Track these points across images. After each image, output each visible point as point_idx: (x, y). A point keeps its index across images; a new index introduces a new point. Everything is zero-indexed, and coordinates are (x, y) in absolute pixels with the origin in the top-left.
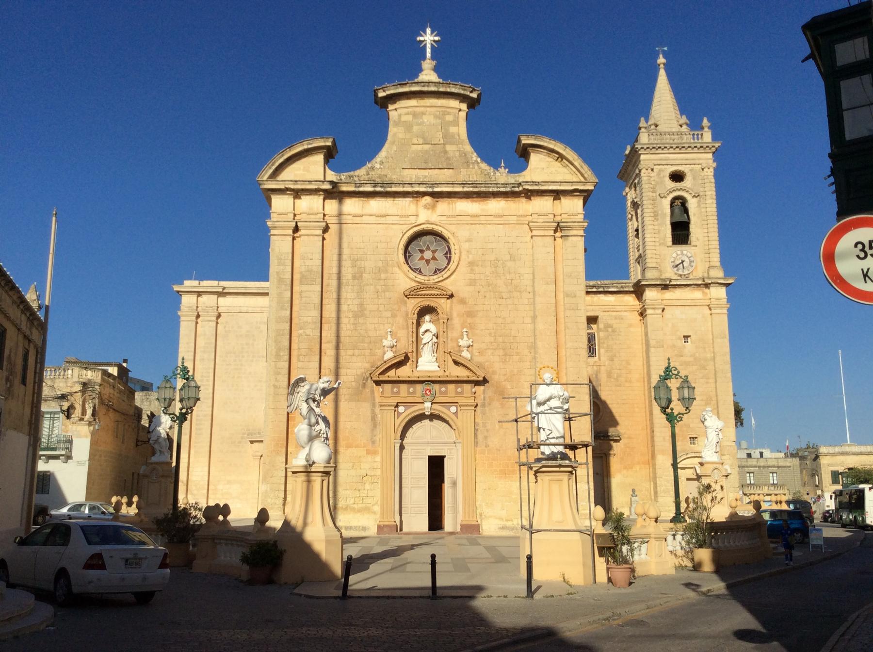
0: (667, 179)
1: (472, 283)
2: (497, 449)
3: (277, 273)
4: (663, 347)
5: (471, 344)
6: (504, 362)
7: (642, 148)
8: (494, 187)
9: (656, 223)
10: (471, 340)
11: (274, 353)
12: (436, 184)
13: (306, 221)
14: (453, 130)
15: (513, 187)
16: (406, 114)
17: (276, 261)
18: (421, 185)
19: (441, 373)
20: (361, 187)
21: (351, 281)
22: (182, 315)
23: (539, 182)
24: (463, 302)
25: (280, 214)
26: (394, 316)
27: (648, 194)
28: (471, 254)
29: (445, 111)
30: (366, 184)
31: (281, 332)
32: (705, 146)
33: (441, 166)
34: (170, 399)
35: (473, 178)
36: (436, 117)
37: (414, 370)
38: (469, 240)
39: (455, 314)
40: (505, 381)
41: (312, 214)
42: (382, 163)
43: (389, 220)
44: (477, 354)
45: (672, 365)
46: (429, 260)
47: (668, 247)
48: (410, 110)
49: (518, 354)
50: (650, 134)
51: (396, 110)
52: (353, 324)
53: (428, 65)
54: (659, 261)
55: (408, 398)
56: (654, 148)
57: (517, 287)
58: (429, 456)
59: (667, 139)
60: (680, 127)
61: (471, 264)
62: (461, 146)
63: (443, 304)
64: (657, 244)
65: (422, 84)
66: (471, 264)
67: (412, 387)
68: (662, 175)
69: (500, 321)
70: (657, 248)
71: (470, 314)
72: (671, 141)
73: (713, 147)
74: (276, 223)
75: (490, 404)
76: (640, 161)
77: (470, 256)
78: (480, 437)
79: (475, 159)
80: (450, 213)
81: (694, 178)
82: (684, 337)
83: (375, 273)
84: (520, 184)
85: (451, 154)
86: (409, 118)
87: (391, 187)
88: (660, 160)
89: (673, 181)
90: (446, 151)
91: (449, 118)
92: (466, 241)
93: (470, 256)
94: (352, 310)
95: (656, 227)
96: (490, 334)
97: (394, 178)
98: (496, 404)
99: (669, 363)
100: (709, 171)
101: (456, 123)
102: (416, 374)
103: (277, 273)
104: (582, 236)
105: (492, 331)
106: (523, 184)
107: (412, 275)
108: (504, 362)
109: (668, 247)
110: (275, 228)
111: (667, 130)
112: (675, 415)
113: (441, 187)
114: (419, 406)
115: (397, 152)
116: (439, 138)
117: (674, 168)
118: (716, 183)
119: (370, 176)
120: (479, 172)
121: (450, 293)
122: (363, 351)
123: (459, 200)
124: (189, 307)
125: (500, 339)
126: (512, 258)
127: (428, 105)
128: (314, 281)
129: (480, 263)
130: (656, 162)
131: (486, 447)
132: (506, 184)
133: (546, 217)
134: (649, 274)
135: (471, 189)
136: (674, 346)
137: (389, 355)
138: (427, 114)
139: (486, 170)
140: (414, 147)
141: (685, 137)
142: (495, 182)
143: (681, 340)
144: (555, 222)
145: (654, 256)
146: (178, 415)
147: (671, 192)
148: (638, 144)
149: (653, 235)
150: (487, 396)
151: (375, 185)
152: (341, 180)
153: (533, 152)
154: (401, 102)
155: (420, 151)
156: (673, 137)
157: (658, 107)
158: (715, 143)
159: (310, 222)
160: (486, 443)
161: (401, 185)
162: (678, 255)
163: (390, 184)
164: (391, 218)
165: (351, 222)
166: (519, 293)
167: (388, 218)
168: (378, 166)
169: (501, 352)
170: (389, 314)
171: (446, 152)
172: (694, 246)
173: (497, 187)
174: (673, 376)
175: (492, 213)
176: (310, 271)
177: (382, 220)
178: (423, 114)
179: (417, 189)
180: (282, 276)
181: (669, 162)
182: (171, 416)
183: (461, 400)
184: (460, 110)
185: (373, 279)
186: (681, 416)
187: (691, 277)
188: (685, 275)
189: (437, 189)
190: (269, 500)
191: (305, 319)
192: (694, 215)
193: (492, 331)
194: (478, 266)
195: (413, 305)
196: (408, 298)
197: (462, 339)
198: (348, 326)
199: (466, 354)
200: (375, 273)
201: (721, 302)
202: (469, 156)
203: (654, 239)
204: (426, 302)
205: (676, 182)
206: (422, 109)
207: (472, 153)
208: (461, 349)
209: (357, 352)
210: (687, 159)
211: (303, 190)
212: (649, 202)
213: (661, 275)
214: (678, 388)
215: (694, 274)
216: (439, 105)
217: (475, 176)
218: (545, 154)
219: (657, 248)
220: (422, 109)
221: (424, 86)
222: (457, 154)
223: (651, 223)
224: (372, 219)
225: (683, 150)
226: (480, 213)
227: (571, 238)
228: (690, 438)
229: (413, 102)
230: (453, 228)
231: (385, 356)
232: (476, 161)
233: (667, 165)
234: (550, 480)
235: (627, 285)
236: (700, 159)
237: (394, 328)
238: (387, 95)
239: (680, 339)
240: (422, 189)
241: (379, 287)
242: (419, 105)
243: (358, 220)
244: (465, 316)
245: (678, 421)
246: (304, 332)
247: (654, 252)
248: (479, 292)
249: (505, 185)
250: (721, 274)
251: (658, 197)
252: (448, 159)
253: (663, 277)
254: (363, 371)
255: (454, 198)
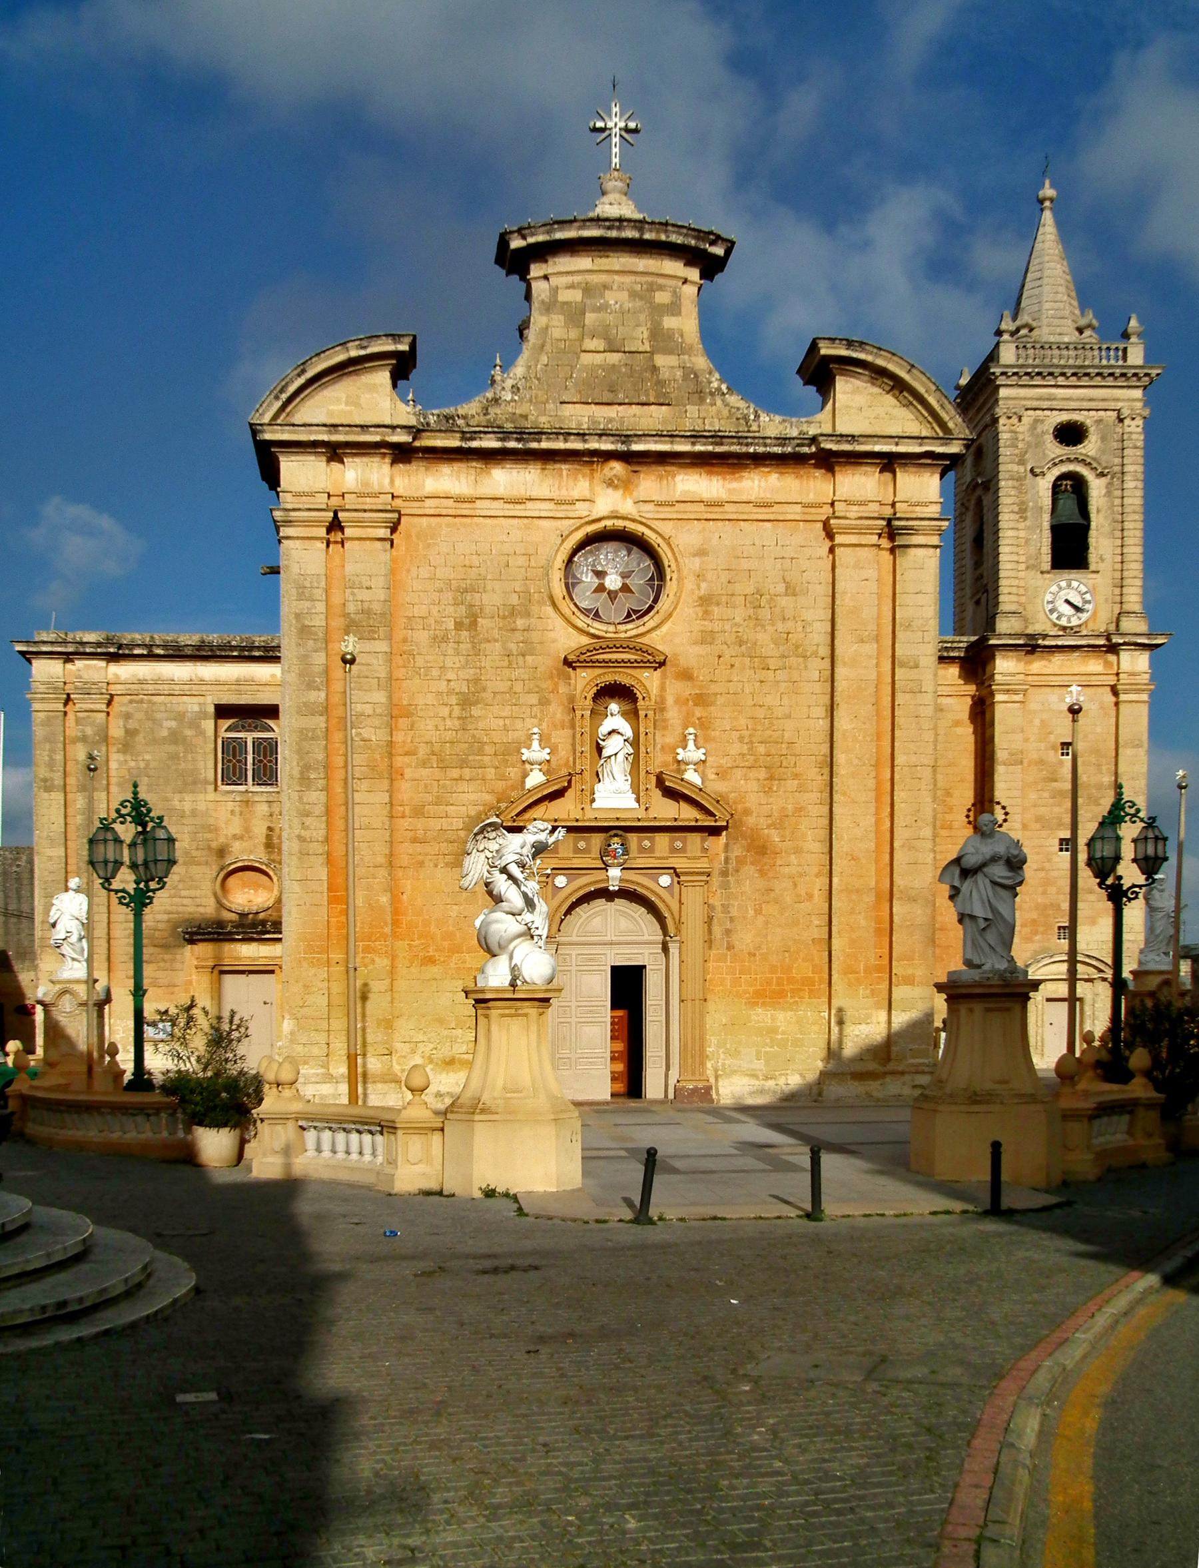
0: (1049, 438)
1: (707, 638)
2: (749, 954)
3: (298, 616)
4: (1021, 763)
5: (703, 758)
6: (768, 791)
7: (1003, 374)
8: (757, 444)
9: (1022, 525)
10: (703, 750)
11: (296, 772)
12: (636, 435)
13: (356, 510)
14: (669, 322)
15: (798, 445)
16: (568, 288)
17: (294, 591)
18: (604, 438)
19: (641, 814)
20: (474, 439)
21: (453, 633)
22: (35, 699)
23: (853, 436)
24: (686, 675)
25: (298, 495)
26: (544, 702)
27: (1010, 467)
28: (704, 580)
29: (652, 284)
30: (485, 433)
31: (310, 734)
32: (1057, 371)
33: (643, 399)
34: (116, 862)
35: (711, 424)
36: (633, 295)
37: (587, 807)
38: (701, 553)
39: (670, 701)
40: (768, 827)
41: (369, 495)
42: (515, 389)
43: (533, 509)
44: (713, 776)
45: (1126, 798)
46: (616, 592)
47: (1042, 573)
48: (577, 279)
49: (796, 776)
50: (1021, 345)
51: (546, 277)
52: (459, 718)
53: (614, 184)
54: (1023, 599)
55: (575, 861)
56: (1027, 374)
57: (797, 647)
58: (614, 969)
59: (1056, 358)
60: (1077, 333)
61: (705, 601)
62: (686, 357)
63: (648, 682)
64: (1022, 567)
65: (607, 224)
66: (705, 601)
67: (583, 839)
68: (1039, 430)
69: (760, 713)
70: (1021, 574)
71: (701, 700)
72: (1062, 362)
73: (1146, 375)
74: (292, 514)
75: (737, 871)
76: (997, 401)
77: (704, 585)
78: (717, 931)
79: (715, 385)
80: (663, 498)
81: (1103, 439)
82: (1063, 744)
83: (504, 617)
84: (814, 440)
85: (665, 374)
86: (576, 296)
87: (539, 441)
88: (1038, 399)
89: (1061, 442)
90: (654, 366)
91: (662, 298)
92: (695, 555)
93: (704, 585)
94: (457, 690)
95: (1022, 534)
96: (741, 739)
97: (544, 422)
98: (749, 870)
99: (1119, 795)
100: (1133, 423)
101: (674, 308)
102: (590, 814)
103: (298, 616)
104: (936, 547)
105: (746, 733)
106: (821, 438)
107: (581, 621)
108: (768, 791)
109: (1042, 573)
110: (288, 523)
111: (1052, 339)
112: (1125, 888)
113: (646, 442)
114: (600, 875)
115: (549, 368)
116: (640, 338)
117: (1064, 417)
118: (1145, 448)
119: (491, 417)
120: (725, 412)
121: (661, 658)
122: (480, 771)
123: (682, 471)
124: (49, 683)
125: (762, 749)
126: (791, 590)
127: (617, 268)
128: (375, 632)
129: (724, 599)
130: (1029, 404)
131: (728, 949)
132: (785, 439)
133: (862, 508)
134: (1002, 625)
135: (710, 448)
136: (1041, 762)
137: (535, 778)
138: (615, 287)
139: (738, 409)
140: (586, 359)
141: (1089, 354)
142: (757, 434)
143: (1056, 751)
144: (883, 519)
145: (1014, 590)
146: (132, 892)
147: (1055, 464)
148: (995, 367)
149: (1015, 549)
150: (733, 855)
151: (505, 435)
152: (428, 424)
153: (841, 375)
154: (556, 260)
155: (599, 366)
156: (1065, 352)
157: (1036, 291)
158: (1151, 368)
159: (365, 511)
160: (728, 942)
161: (561, 437)
162: (1060, 588)
163: (539, 434)
164: (539, 505)
165: (450, 512)
166: (801, 660)
167: (529, 505)
168: (508, 396)
169: (762, 774)
170: (533, 699)
171: (655, 369)
172: (1094, 572)
173: (765, 445)
174: (1127, 818)
175: (753, 498)
176: (368, 612)
177: (518, 510)
178: (606, 287)
179: (594, 445)
180: (307, 623)
181: (1055, 404)
182: (120, 894)
183: (680, 863)
184: (685, 281)
185: (500, 629)
186: (1137, 889)
187: (1084, 632)
188: (1072, 628)
189: (637, 447)
190: (299, 1048)
191: (359, 708)
192: (1098, 511)
193: (746, 733)
194: (718, 604)
195: (585, 681)
196: (574, 668)
197: (684, 748)
198: (448, 723)
199: (692, 776)
200: (504, 617)
201: (1138, 680)
202: (702, 379)
203: (1015, 558)
204: (610, 677)
205: (1068, 445)
206: (603, 278)
207: (710, 373)
208: (683, 767)
209: (467, 772)
210: (1091, 400)
211: (348, 444)
212: (1010, 483)
213: (1026, 627)
214: (1134, 841)
215: (1091, 626)
216: (641, 269)
217: (716, 420)
218: (866, 378)
219: (1021, 574)
220: (603, 278)
221: (609, 228)
222: (679, 374)
223: (1012, 525)
224: (497, 508)
225: (1085, 381)
226: (724, 496)
227: (913, 551)
228: (1059, 928)
229: (583, 262)
230: (667, 528)
231: (527, 780)
232: (719, 389)
233: (1052, 410)
234: (988, 1010)
235: (955, 645)
236: (1117, 400)
237: (544, 726)
238: (530, 246)
239: (1054, 748)
240: (606, 446)
241: (513, 647)
242: (595, 268)
243: (465, 509)
244: (691, 703)
245: (1130, 900)
246: (359, 734)
247: (1016, 582)
248: (720, 657)
249: (783, 440)
250: (1143, 627)
251: (1029, 475)
252: (660, 383)
253: (1029, 631)
254: (481, 808)
255: (673, 464)
